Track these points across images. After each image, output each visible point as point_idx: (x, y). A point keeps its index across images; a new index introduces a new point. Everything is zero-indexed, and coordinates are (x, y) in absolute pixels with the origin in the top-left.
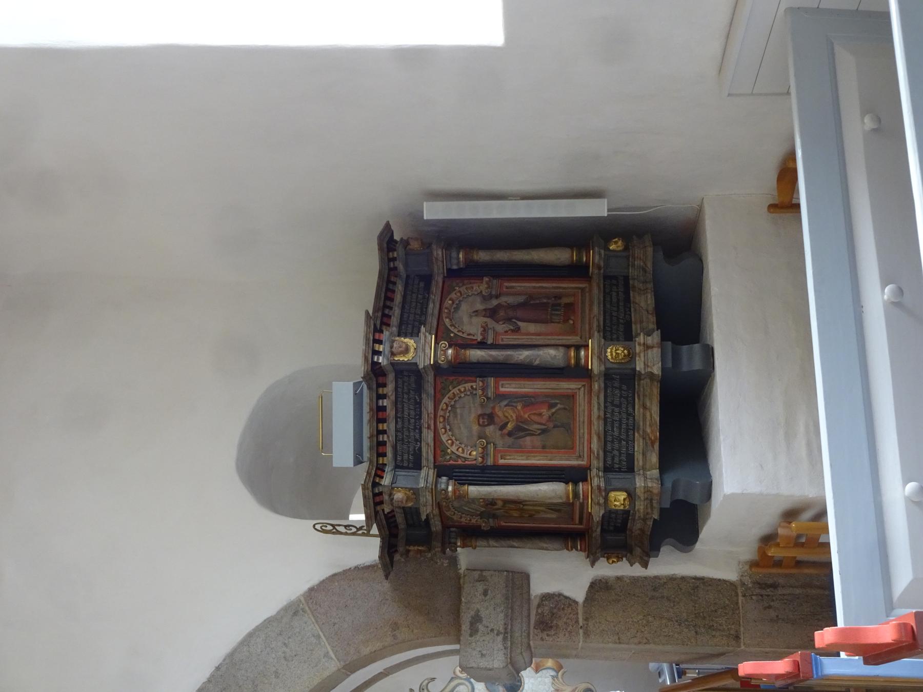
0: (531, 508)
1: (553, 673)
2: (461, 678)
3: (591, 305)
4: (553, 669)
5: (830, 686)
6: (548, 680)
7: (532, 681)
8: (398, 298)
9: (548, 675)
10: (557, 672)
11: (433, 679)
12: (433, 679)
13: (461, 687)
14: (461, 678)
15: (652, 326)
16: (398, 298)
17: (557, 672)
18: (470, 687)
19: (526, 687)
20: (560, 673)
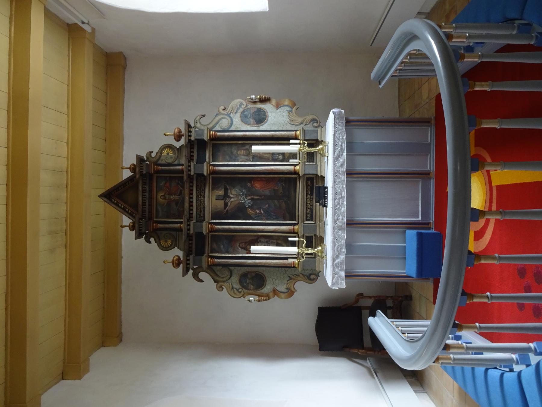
0: (194, 208)
1: (289, 109)
2: (223, 114)
3: (144, 204)
4: (289, 106)
5: (409, 126)
6: (285, 114)
7: (274, 114)
8: (195, 197)
9: (285, 110)
10: (292, 108)
11: (204, 116)
12: (204, 116)
13: (224, 120)
14: (223, 114)
15: (473, 82)
16: (195, 197)
17: (292, 108)
18: (230, 120)
19: (269, 119)
20: (294, 109)
